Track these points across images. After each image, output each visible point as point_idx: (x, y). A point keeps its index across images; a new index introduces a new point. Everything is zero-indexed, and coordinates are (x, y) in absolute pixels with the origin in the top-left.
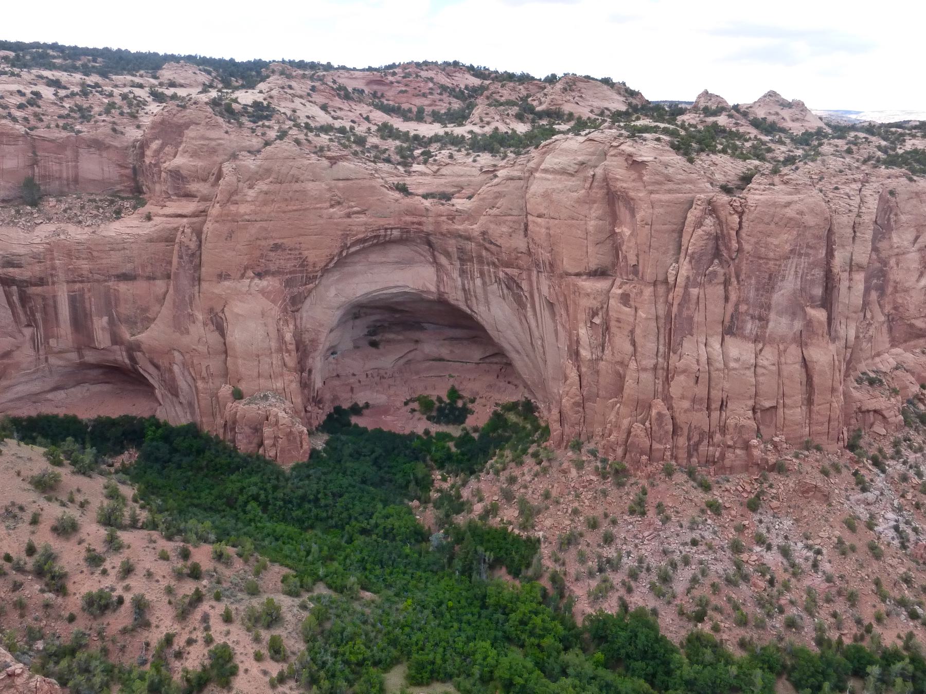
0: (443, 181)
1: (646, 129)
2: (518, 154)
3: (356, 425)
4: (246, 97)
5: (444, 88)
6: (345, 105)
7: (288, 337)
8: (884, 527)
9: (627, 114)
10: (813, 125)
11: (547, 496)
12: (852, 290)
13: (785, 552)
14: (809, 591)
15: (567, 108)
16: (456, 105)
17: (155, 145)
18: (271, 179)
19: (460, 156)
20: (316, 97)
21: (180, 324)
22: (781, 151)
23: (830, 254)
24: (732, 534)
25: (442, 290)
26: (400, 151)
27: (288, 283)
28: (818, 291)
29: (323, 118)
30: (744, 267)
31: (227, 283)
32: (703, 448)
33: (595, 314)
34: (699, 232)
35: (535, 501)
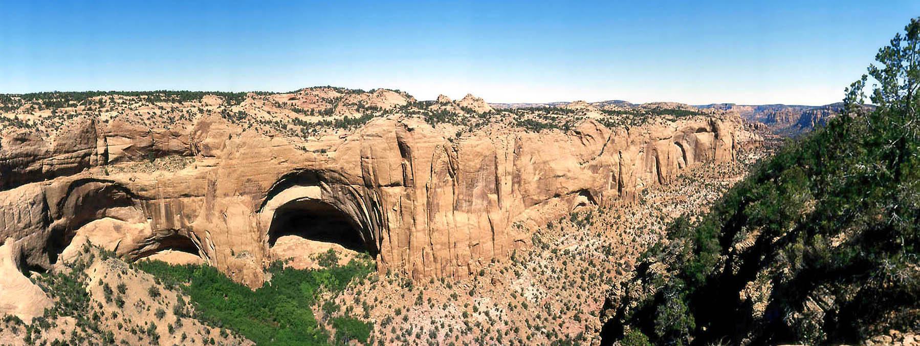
0: (322, 144)
1: (414, 113)
2: (356, 128)
4: (236, 109)
5: (323, 99)
6: (278, 110)
7: (254, 224)
8: (529, 295)
9: (406, 107)
10: (487, 109)
11: (376, 300)
12: (506, 185)
13: (487, 314)
14: (498, 331)
15: (379, 105)
16: (329, 106)
17: (199, 133)
19: (330, 131)
20: (265, 108)
21: (208, 218)
22: (474, 121)
23: (496, 168)
24: (463, 309)
26: (302, 130)
27: (254, 198)
28: (493, 186)
29: (267, 117)
30: (460, 178)
31: (228, 198)
32: (448, 268)
33: (395, 205)
34: (439, 161)
35: (370, 302)
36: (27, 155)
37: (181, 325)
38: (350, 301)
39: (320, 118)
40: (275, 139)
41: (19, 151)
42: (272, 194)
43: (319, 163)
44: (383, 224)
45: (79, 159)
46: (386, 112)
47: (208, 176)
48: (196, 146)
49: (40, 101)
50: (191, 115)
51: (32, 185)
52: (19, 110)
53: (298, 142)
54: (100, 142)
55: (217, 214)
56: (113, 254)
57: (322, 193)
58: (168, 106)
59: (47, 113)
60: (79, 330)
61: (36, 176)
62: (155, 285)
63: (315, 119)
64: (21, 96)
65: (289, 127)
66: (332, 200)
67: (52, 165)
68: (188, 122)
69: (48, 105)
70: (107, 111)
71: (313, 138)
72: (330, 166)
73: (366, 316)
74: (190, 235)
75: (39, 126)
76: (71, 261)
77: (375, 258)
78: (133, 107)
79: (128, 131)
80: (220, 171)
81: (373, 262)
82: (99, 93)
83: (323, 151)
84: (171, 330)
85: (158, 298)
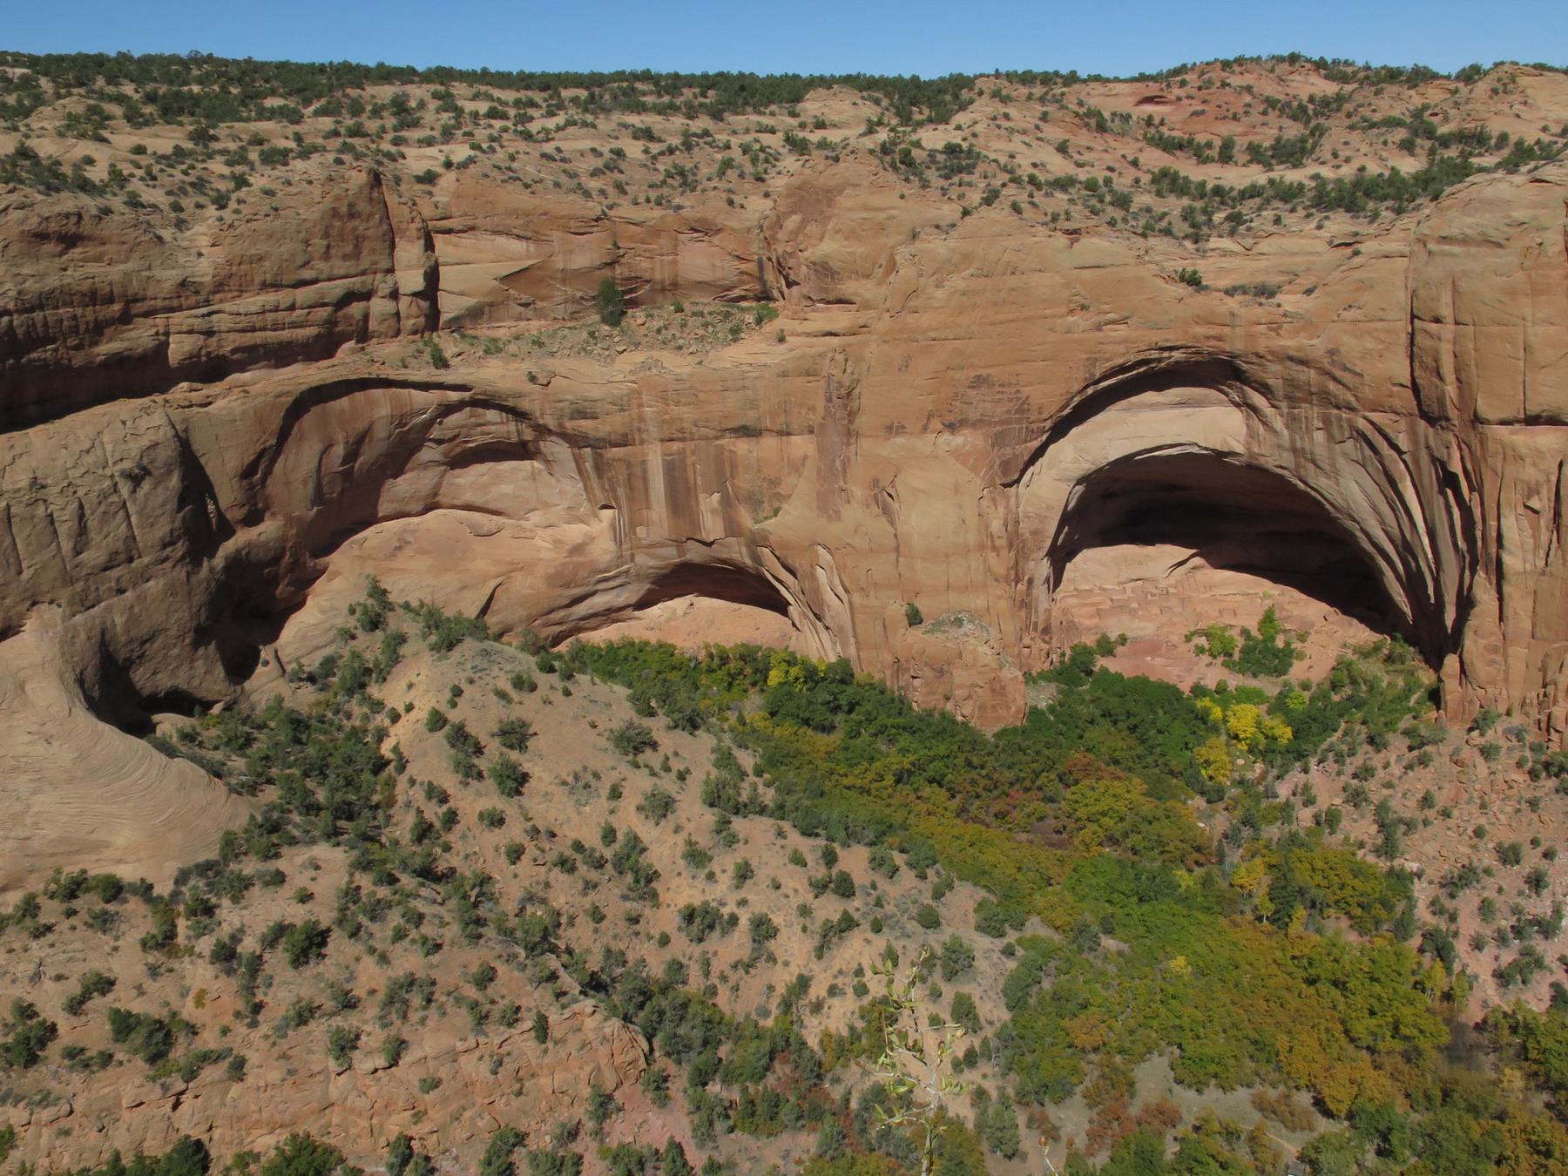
0: (1263, 264)
3: (1105, 671)
4: (933, 138)
5: (1271, 103)
6: (1098, 143)
11: (1427, 801)
15: (1495, 127)
16: (1293, 130)
17: (792, 222)
18: (971, 271)
21: (826, 504)
25: (1256, 450)
29: (1059, 166)
31: (900, 440)
33: (1533, 491)
35: (1404, 806)
36: (92, 297)
37: (732, 841)
38: (1328, 794)
39: (1257, 175)
40: (1086, 242)
41: (53, 282)
42: (1060, 429)
43: (1243, 329)
44: (1481, 552)
45: (323, 313)
46: (1521, 155)
47: (826, 368)
48: (780, 268)
49: (128, 89)
50: (763, 160)
51: (123, 408)
52: (35, 122)
53: (1172, 255)
54: (409, 252)
55: (858, 492)
56: (478, 627)
57: (1252, 433)
58: (672, 127)
59: (164, 139)
60: (365, 881)
61: (143, 375)
62: (637, 720)
63: (1237, 177)
64: (33, 62)
65: (1142, 199)
66: (1287, 459)
67: (209, 333)
68: (748, 185)
69: (171, 110)
70: (429, 142)
71: (1226, 243)
72: (1289, 342)
73: (1388, 849)
74: (756, 558)
75: (136, 185)
76: (313, 663)
77: (1435, 663)
78: (534, 127)
79: (515, 213)
80: (873, 350)
81: (1426, 677)
82: (385, 74)
83: (1266, 292)
84: (696, 857)
85: (647, 755)
